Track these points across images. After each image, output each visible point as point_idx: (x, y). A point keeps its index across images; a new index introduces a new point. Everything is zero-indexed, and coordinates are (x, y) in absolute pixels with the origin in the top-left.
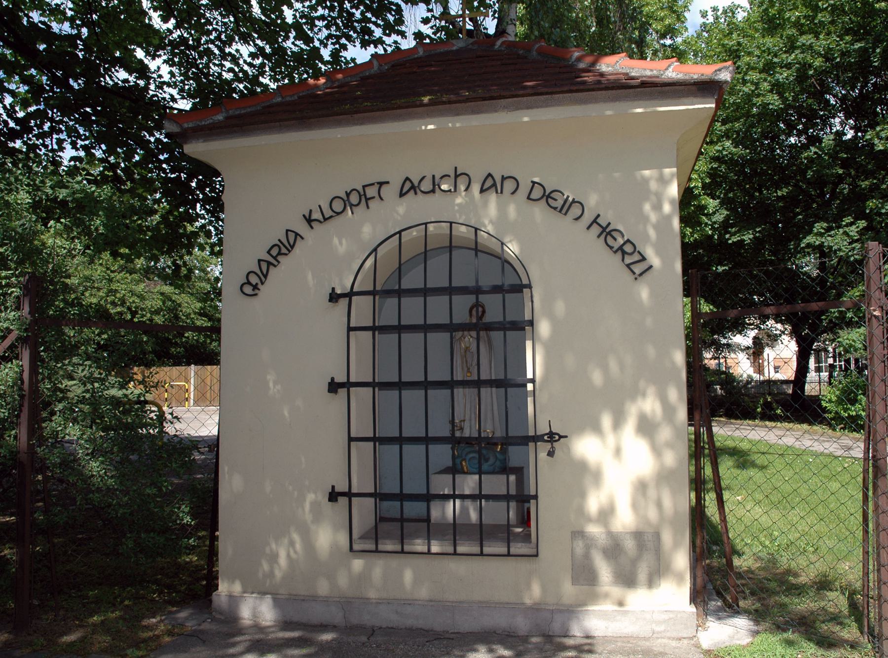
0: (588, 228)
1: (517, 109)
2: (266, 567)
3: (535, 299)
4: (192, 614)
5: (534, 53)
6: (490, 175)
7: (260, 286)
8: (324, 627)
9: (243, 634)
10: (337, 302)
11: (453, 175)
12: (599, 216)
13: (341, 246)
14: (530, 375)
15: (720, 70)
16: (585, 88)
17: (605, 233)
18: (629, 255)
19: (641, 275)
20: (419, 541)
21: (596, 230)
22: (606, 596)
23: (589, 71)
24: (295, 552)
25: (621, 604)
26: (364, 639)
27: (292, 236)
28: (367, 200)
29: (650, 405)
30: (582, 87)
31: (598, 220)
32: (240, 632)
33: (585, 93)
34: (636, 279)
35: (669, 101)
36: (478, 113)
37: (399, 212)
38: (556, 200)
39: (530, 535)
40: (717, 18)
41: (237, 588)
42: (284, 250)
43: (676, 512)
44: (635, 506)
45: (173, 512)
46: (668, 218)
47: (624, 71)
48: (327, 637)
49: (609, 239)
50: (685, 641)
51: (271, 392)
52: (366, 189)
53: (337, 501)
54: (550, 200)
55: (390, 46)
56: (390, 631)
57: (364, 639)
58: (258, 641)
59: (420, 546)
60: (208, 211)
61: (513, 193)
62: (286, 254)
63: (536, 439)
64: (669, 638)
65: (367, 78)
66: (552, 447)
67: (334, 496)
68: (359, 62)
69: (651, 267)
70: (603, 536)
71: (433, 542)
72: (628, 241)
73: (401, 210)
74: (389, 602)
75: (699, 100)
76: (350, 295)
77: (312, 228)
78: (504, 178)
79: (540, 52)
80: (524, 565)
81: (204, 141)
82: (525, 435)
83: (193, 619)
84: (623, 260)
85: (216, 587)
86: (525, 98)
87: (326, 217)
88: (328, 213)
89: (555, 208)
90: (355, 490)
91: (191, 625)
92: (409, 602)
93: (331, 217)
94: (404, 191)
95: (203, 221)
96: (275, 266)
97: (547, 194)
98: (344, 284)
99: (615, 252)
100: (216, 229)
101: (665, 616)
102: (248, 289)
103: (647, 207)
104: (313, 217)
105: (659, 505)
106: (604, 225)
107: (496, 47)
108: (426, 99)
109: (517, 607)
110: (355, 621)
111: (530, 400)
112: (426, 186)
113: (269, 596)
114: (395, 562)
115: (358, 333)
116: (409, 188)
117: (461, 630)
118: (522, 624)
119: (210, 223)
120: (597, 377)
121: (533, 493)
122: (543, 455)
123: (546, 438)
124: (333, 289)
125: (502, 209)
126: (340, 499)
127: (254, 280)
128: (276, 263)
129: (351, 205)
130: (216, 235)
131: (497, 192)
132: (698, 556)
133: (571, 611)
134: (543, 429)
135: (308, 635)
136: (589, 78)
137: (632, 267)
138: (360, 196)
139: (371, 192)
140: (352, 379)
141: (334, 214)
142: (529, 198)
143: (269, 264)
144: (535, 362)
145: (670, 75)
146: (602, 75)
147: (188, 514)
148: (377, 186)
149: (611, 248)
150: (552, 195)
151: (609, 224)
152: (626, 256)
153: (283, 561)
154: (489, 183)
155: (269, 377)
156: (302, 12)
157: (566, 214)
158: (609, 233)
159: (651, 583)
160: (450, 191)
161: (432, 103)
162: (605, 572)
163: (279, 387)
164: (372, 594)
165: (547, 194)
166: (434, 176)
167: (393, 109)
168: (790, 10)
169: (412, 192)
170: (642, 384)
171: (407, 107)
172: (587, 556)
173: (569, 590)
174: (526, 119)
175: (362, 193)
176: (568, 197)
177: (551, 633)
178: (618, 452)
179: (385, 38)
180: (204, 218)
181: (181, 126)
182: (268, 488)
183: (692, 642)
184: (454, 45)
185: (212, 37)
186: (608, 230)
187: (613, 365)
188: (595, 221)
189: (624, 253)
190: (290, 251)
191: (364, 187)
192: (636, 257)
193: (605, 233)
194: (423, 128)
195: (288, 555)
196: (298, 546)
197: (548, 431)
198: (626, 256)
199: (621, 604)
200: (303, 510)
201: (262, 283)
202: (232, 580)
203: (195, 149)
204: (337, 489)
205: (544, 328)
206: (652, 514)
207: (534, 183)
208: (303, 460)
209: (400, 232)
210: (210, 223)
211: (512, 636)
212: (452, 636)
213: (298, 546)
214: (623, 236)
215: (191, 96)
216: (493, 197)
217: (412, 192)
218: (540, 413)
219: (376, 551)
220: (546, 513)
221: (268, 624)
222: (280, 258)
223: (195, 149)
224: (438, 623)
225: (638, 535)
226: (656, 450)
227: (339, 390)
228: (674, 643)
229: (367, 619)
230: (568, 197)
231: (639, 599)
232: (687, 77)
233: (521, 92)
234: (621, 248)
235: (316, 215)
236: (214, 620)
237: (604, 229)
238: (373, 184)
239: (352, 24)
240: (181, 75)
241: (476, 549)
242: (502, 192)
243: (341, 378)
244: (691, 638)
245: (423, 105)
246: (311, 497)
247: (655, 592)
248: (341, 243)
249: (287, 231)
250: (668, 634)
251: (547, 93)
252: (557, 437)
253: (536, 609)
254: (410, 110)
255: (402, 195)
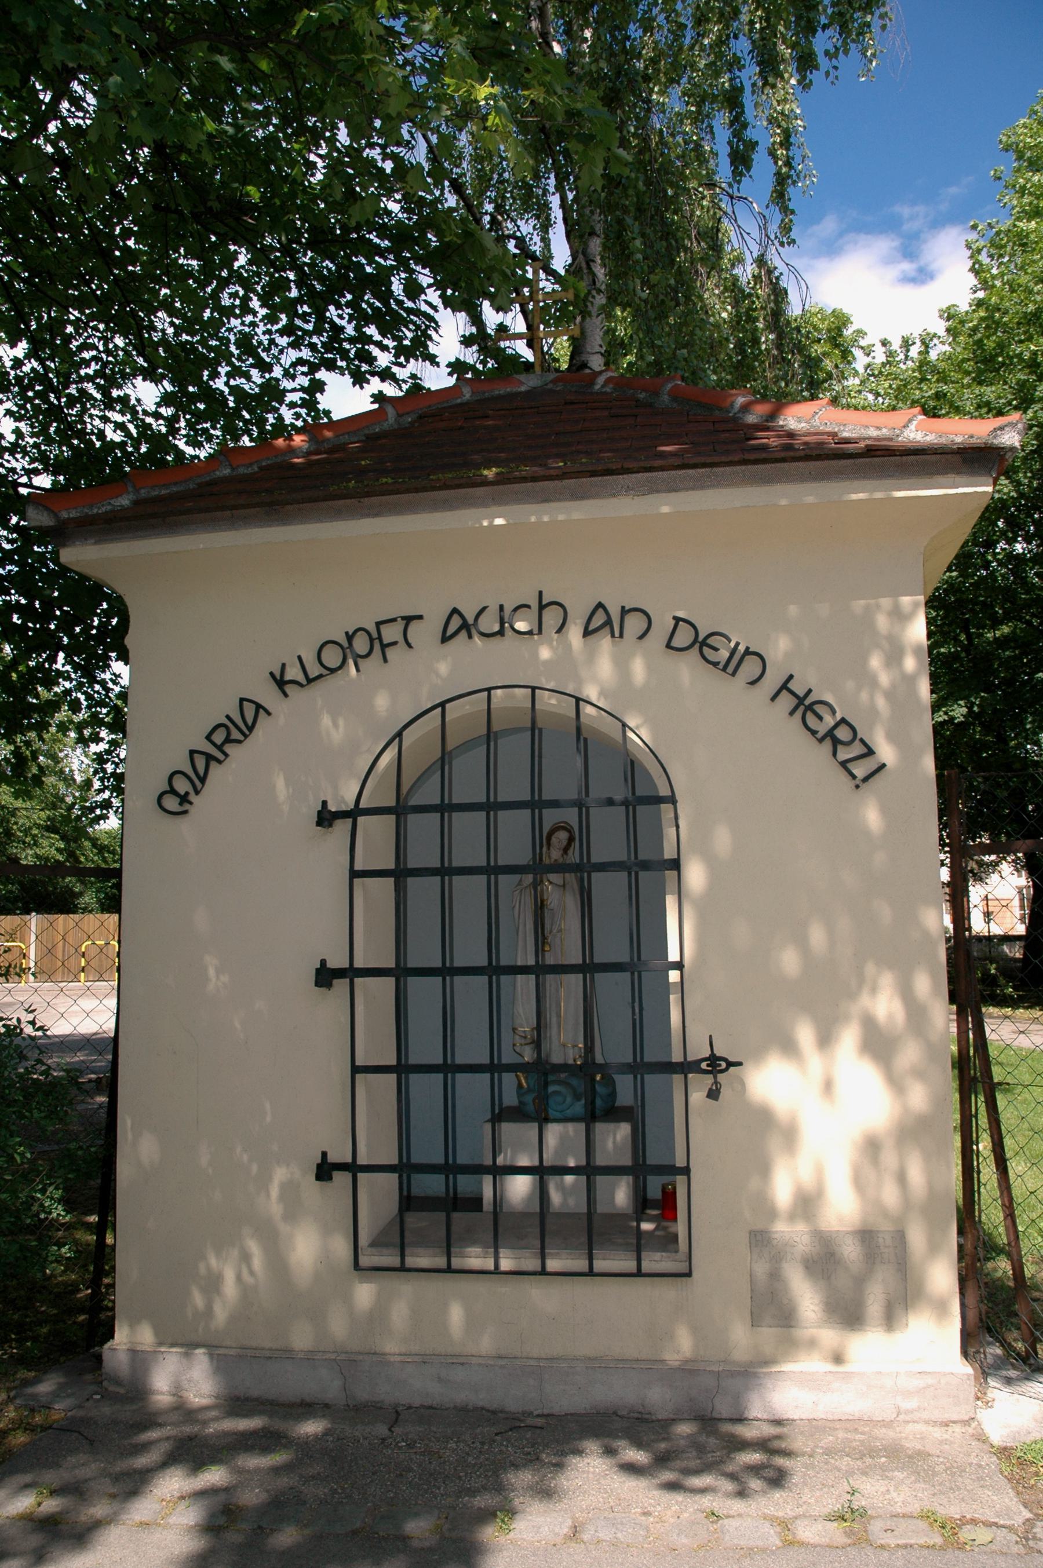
0: (773, 699)
1: (651, 491)
2: (198, 1299)
3: (682, 823)
4: (61, 1387)
5: (666, 398)
6: (600, 605)
7: (192, 797)
8: (307, 1408)
9: (160, 1425)
10: (330, 825)
11: (535, 605)
12: (791, 677)
13: (334, 729)
14: (673, 956)
15: (1001, 428)
16: (763, 457)
17: (802, 708)
18: (843, 743)
19: (866, 779)
20: (476, 1250)
21: (786, 701)
22: (812, 1344)
23: (767, 429)
24: (252, 1273)
25: (838, 1358)
26: (382, 1430)
27: (249, 710)
28: (384, 647)
29: (885, 1005)
30: (764, 455)
31: (790, 685)
32: (150, 1420)
33: (768, 466)
34: (857, 787)
35: (927, 481)
36: (582, 498)
37: (439, 670)
38: (716, 649)
39: (675, 1238)
40: (891, 354)
41: (146, 1336)
42: (236, 735)
43: (932, 1192)
44: (858, 1182)
45: (33, 1198)
46: (910, 680)
47: (829, 429)
48: (311, 1428)
49: (811, 719)
50: (958, 1429)
51: (211, 987)
52: (382, 627)
53: (330, 1178)
54: (706, 650)
55: (404, 381)
56: (428, 1413)
57: (382, 1430)
58: (190, 1438)
59: (476, 1258)
60: (76, 667)
61: (641, 637)
62: (239, 742)
63: (687, 1067)
64: (927, 1422)
65: (377, 437)
66: (716, 1083)
67: (325, 1170)
68: (335, 417)
69: (884, 766)
70: (806, 1239)
71: (502, 1252)
72: (843, 721)
73: (443, 668)
74: (424, 1360)
75: (964, 479)
76: (354, 814)
77: (286, 695)
78: (624, 612)
79: (674, 395)
80: (665, 1292)
81: (96, 543)
82: (667, 1060)
83: (68, 1396)
84: (835, 754)
85: (111, 1336)
86: (665, 474)
87: (311, 676)
88: (314, 670)
89: (715, 664)
90: (362, 1160)
91: (61, 1409)
92: (458, 1361)
93: (320, 676)
94: (448, 634)
95: (67, 685)
96: (220, 762)
97: (700, 639)
98: (346, 795)
99: (821, 740)
100: (89, 697)
101: (919, 1382)
102: (172, 803)
103: (875, 662)
104: (288, 677)
105: (902, 1178)
106: (801, 693)
107: (597, 387)
108: (490, 473)
109: (651, 1368)
110: (363, 1394)
111: (674, 999)
112: (489, 623)
113: (200, 1351)
114: (433, 1287)
115: (368, 881)
116: (458, 626)
117: (556, 1410)
118: (658, 1398)
119: (79, 687)
120: (790, 961)
121: (680, 1163)
122: (698, 1097)
123: (704, 1065)
124: (324, 803)
125: (622, 665)
126: (337, 1175)
127: (182, 786)
128: (221, 757)
129: (357, 657)
130: (89, 707)
131: (613, 636)
132: (970, 1274)
133: (750, 1373)
134: (699, 1050)
135: (279, 1425)
136: (772, 441)
137: (850, 766)
138: (372, 640)
139: (391, 633)
140: (359, 964)
141: (325, 672)
142: (668, 646)
143: (209, 758)
144: (679, 936)
145: (912, 436)
146: (791, 435)
147: (59, 1201)
148: (400, 625)
149: (814, 733)
150: (709, 641)
151: (810, 691)
152: (840, 748)
153: (230, 1288)
154: (599, 620)
155: (208, 959)
156: (240, 332)
157: (733, 674)
158: (810, 708)
159: (890, 1320)
160: (530, 633)
161: (501, 480)
162: (808, 1300)
163: (225, 978)
164: (391, 1347)
165: (700, 639)
166: (501, 607)
167: (434, 489)
168: (1021, 342)
169: (463, 634)
170: (870, 968)
171: (459, 486)
172: (775, 1276)
173: (741, 1339)
174: (665, 509)
175: (375, 635)
176: (737, 644)
177: (715, 1415)
178: (828, 1086)
179: (395, 369)
180: (69, 679)
181: (56, 515)
182: (204, 1160)
183: (970, 1430)
184: (522, 383)
185: (90, 371)
186: (807, 702)
187: (817, 936)
188: (785, 687)
189: (836, 742)
190: (246, 736)
191: (378, 624)
192: (857, 749)
193: (802, 708)
194: (533, 519)
195: (239, 1278)
196: (257, 1262)
197: (707, 1053)
198: (840, 748)
199: (838, 1358)
200: (268, 1195)
201: (197, 792)
202: (133, 1323)
203: (82, 556)
204: (332, 1158)
205: (695, 875)
206: (890, 1195)
207: (677, 620)
208: (268, 1106)
209: (442, 705)
210: (79, 687)
211: (646, 1421)
212: (540, 1422)
213: (257, 1262)
214: (833, 712)
215: (53, 468)
216: (605, 642)
217: (463, 634)
218: (693, 1022)
219: (403, 1269)
220: (705, 1200)
221: (205, 1402)
222: (228, 748)
223: (82, 556)
224: (514, 1397)
225: (866, 1235)
226: (895, 1083)
227: (335, 982)
228: (938, 1433)
229: (386, 1393)
230: (737, 644)
231: (869, 1347)
232: (943, 440)
233: (658, 463)
234: (830, 734)
235: (293, 673)
236: (106, 1396)
237: (801, 700)
238: (394, 620)
239: (341, 345)
240: (33, 435)
241: (531, 1263)
242: (621, 636)
243: (338, 961)
244: (967, 1423)
245: (485, 483)
246: (280, 1174)
247: (898, 1337)
248: (335, 725)
249: (242, 700)
250: (925, 1415)
251: (704, 465)
252: (724, 1065)
253: (688, 1370)
254: (463, 491)
255: (445, 639)
